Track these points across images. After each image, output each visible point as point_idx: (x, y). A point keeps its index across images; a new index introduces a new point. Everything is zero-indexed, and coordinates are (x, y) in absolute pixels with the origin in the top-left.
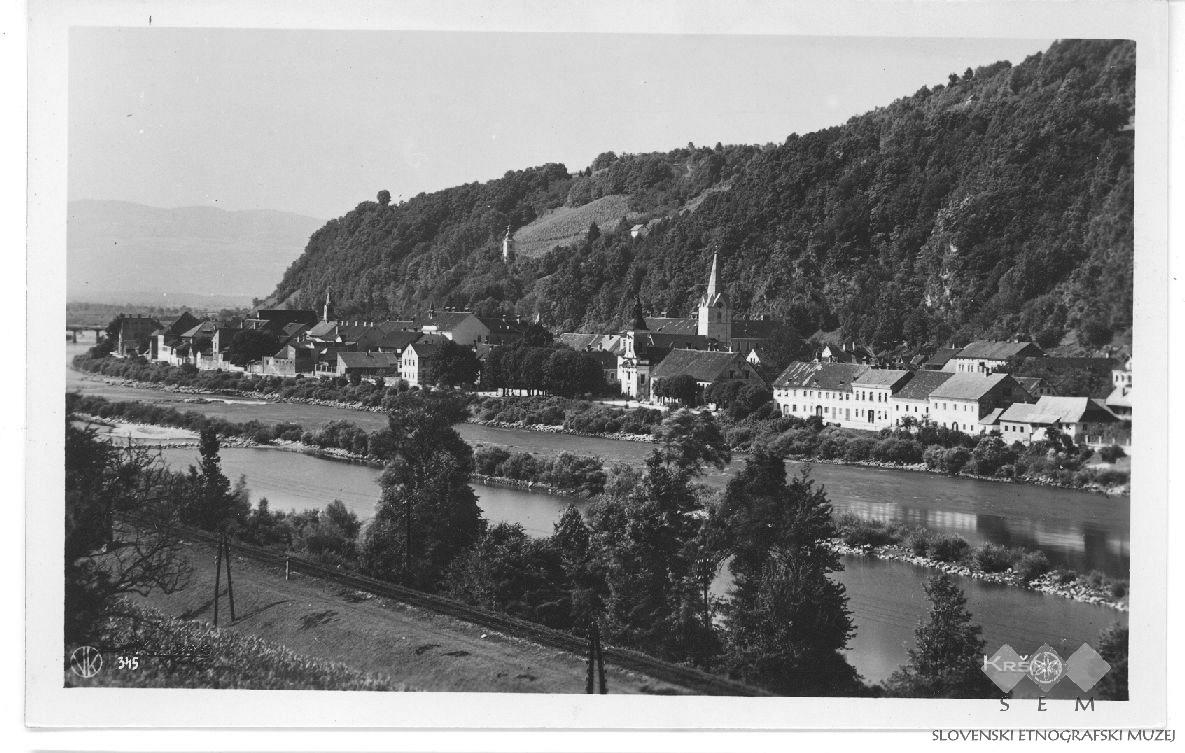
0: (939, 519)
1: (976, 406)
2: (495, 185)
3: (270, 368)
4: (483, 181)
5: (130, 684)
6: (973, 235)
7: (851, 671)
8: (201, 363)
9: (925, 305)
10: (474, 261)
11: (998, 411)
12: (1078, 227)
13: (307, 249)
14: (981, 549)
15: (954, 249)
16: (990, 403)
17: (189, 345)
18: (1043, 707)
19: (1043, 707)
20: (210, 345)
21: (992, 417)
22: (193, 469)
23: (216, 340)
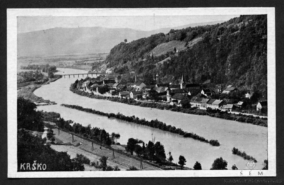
0: (28, 150)
1: (218, 106)
2: (150, 38)
3: (107, 95)
4: (147, 37)
5: (192, 113)
6: (233, 62)
7: (149, 143)
8: (95, 93)
9: (225, 75)
10: (130, 164)
11: (221, 106)
12: (250, 61)
13: (128, 117)
14: (47, 141)
15: (230, 65)
16: (220, 105)
17: (92, 89)
18: (250, 174)
19: (250, 174)
20: (96, 89)
21: (221, 107)
22: (185, 164)
23: (97, 89)
